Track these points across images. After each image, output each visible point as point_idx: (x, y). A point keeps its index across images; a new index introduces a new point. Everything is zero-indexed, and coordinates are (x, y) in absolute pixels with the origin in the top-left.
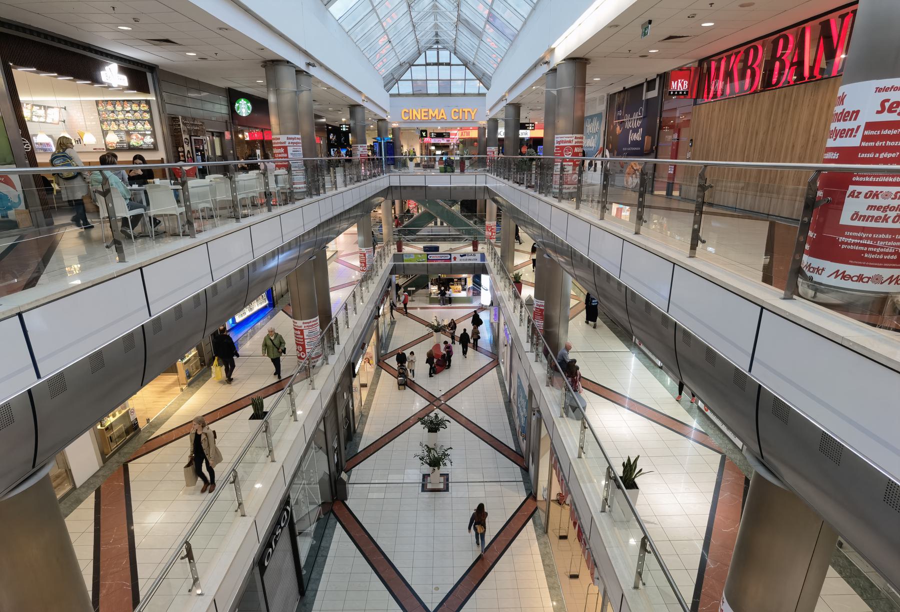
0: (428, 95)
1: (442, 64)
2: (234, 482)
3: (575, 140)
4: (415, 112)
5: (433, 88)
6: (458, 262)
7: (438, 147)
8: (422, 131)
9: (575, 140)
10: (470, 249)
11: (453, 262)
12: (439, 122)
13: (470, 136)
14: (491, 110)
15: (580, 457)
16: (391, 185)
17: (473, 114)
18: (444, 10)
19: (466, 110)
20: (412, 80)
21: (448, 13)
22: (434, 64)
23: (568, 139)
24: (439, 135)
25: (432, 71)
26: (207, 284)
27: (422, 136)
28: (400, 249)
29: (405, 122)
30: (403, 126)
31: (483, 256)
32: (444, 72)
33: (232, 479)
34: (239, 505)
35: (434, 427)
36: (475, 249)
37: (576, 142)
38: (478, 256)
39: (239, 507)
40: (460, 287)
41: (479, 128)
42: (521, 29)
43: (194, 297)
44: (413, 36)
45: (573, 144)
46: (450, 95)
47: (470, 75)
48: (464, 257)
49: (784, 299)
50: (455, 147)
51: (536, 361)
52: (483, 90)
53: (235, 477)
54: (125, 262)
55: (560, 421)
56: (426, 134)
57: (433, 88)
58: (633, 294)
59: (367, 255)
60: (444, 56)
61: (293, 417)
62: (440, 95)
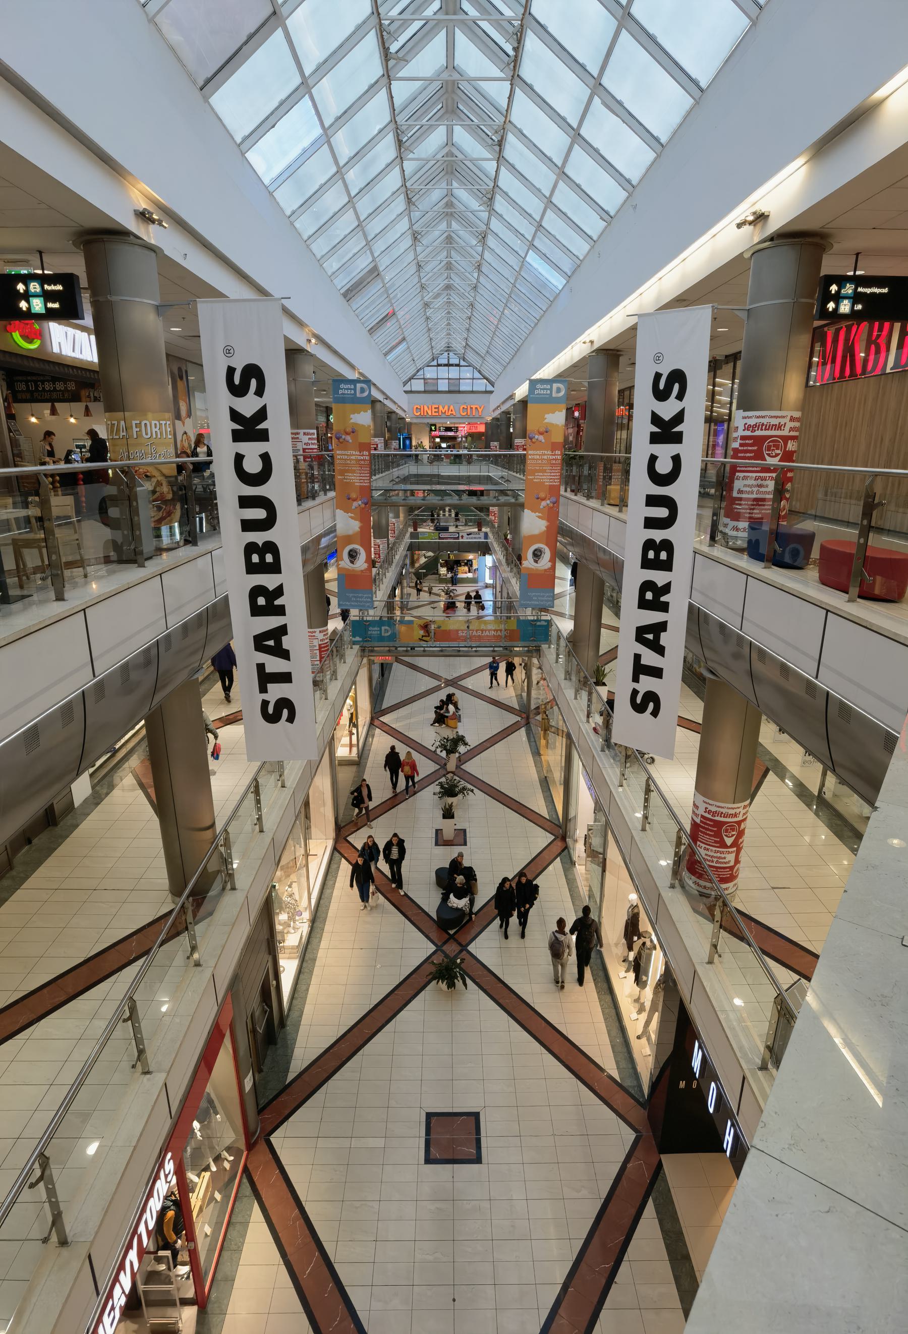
0: (438, 392)
1: (452, 365)
2: (130, 1018)
3: (790, 425)
4: (426, 408)
5: (443, 386)
6: (465, 540)
7: (443, 439)
8: (432, 425)
9: (790, 425)
10: (476, 530)
11: (461, 540)
12: (448, 417)
13: (478, 430)
14: (494, 411)
15: (644, 830)
16: (411, 473)
17: (480, 410)
18: (463, 244)
19: (474, 407)
20: (424, 379)
21: (467, 274)
22: (445, 365)
23: (774, 421)
24: (448, 429)
25: (443, 372)
26: (84, 681)
27: (431, 430)
28: (415, 529)
29: (417, 417)
30: (415, 421)
31: (486, 535)
32: (454, 373)
33: (127, 1014)
34: (139, 1056)
35: (453, 744)
36: (480, 530)
37: (791, 429)
38: (482, 535)
39: (139, 1059)
40: (466, 568)
41: (486, 424)
42: (573, 273)
43: (122, 666)
44: (416, 280)
45: (785, 432)
46: (459, 392)
47: (477, 375)
48: (470, 536)
49: (849, 601)
50: (464, 439)
51: (566, 679)
52: (490, 388)
53: (133, 1009)
54: (144, 567)
55: (602, 756)
56: (435, 428)
57: (443, 386)
58: (845, 711)
59: (381, 547)
60: (454, 361)
61: (258, 826)
62: (449, 392)
